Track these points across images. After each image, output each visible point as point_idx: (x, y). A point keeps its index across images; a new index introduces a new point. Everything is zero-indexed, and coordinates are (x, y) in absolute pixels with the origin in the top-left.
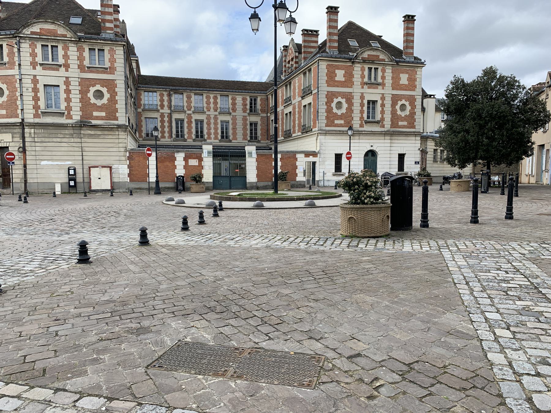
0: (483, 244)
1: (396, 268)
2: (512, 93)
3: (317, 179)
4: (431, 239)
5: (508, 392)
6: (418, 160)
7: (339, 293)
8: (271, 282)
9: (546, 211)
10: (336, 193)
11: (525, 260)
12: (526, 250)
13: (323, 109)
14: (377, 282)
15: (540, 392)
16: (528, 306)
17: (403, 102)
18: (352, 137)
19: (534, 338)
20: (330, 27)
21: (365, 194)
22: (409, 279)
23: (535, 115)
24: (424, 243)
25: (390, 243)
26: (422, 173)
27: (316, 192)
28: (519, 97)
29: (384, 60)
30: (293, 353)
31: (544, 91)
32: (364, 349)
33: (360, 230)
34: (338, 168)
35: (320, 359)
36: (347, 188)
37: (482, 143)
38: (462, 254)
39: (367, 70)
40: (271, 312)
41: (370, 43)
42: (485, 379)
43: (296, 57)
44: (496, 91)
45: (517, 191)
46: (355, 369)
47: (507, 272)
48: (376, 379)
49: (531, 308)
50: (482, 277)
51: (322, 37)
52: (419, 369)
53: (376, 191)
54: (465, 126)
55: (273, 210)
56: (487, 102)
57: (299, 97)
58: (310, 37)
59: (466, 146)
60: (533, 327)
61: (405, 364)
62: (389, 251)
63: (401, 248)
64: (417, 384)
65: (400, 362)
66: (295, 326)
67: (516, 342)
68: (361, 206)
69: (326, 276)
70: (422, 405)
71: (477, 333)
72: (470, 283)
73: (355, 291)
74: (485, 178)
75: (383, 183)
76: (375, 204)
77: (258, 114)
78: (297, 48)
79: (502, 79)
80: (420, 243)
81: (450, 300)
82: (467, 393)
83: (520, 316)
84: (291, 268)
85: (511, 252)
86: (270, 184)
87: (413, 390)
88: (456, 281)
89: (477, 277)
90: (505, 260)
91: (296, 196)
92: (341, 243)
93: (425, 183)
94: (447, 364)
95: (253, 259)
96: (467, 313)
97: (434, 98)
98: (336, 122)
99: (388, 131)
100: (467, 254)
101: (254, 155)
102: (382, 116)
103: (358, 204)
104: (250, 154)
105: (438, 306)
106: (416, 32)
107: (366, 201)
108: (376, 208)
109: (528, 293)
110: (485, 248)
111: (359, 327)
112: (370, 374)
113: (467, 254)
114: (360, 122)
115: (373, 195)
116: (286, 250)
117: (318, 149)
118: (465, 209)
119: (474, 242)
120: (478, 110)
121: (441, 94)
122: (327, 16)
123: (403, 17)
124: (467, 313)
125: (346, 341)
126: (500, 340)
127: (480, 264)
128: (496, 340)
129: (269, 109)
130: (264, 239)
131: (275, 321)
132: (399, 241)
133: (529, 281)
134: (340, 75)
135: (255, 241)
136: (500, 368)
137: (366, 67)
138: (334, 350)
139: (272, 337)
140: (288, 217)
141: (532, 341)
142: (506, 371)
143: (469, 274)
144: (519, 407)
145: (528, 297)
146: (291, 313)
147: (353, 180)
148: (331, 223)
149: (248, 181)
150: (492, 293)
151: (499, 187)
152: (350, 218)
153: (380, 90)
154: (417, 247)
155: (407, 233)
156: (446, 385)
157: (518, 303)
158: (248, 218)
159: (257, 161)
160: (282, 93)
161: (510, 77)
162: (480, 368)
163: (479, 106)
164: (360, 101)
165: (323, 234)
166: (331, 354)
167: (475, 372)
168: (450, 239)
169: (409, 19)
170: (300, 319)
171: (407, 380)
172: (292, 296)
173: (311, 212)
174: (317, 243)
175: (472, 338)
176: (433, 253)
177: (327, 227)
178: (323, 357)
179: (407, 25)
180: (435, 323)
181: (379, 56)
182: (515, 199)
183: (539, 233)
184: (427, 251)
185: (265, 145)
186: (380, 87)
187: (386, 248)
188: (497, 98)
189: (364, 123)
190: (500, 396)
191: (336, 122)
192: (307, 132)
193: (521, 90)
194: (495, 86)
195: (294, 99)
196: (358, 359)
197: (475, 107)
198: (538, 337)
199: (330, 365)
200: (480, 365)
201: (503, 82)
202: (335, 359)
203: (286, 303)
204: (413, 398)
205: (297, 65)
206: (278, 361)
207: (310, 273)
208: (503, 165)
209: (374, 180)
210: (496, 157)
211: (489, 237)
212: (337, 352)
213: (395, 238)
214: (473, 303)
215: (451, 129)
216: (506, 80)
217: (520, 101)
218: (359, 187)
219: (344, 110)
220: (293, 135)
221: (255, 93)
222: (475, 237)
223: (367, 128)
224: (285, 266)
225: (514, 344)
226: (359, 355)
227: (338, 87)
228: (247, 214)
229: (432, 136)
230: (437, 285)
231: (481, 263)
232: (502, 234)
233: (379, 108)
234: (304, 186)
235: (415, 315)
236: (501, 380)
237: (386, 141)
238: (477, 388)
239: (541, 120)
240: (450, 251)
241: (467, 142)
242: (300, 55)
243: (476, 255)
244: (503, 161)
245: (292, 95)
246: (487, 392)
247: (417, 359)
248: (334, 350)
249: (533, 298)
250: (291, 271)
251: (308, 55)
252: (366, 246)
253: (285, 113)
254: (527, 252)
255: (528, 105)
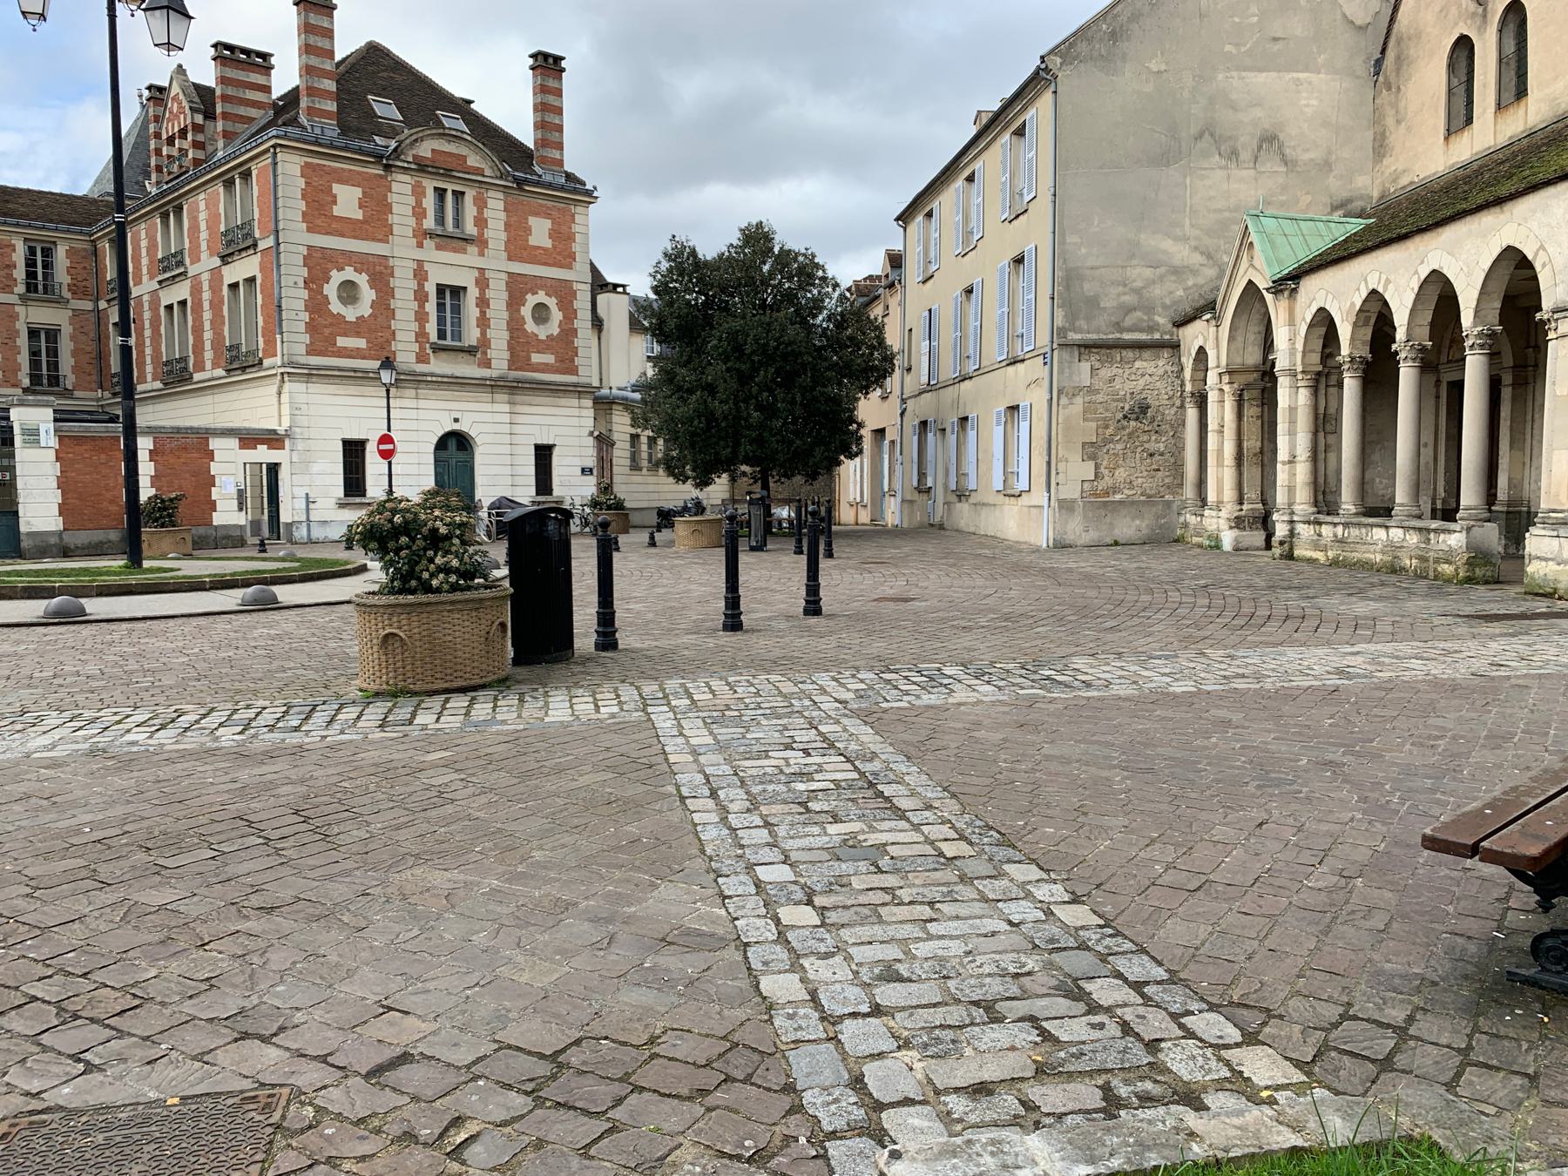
0: (752, 685)
1: (525, 776)
2: (809, 295)
3: (285, 517)
4: (623, 682)
5: (808, 1075)
6: (591, 462)
7: (347, 873)
8: (104, 871)
9: (891, 592)
10: (347, 563)
11: (846, 715)
12: (848, 690)
13: (295, 300)
14: (467, 823)
15: (880, 1055)
16: (854, 835)
17: (541, 297)
18: (393, 391)
19: (867, 917)
20: (307, 49)
21: (431, 561)
22: (560, 801)
23: (863, 355)
24: (606, 695)
25: (510, 703)
26: (603, 499)
27: (283, 560)
28: (825, 308)
29: (480, 172)
30: (176, 1101)
31: (877, 297)
32: (422, 1035)
33: (419, 670)
34: (354, 483)
35: (275, 1099)
36: (374, 545)
37: (746, 420)
38: (701, 714)
39: (430, 193)
40: (98, 976)
41: (437, 116)
42: (754, 1049)
43: (198, 128)
44: (774, 287)
45: (829, 544)
46: (392, 1106)
47: (807, 752)
48: (458, 1122)
49: (861, 837)
50: (750, 772)
51: (285, 77)
52: (584, 1063)
53: (466, 551)
54: (703, 373)
55: (125, 625)
56: (754, 315)
57: (211, 255)
58: (243, 70)
59: (709, 428)
60: (865, 886)
61: (541, 1056)
62: (506, 727)
63: (541, 714)
64: (575, 1108)
65: (530, 1053)
66: (189, 1008)
67: (827, 936)
68: (423, 598)
69: (304, 827)
70: (588, 1168)
71: (736, 927)
72: (720, 792)
73: (398, 862)
74: (758, 512)
75: (494, 529)
76: (462, 589)
77: (60, 302)
78: (197, 99)
79: (786, 257)
80: (593, 695)
81: (670, 847)
82: (710, 1100)
83: (837, 864)
84: (180, 814)
85: (817, 699)
86: (114, 535)
87: (574, 1130)
88: (685, 791)
89: (736, 774)
90: (802, 720)
91: (209, 576)
92: (359, 717)
93: (605, 525)
94: (658, 1032)
95: (33, 800)
96: (712, 876)
97: (625, 292)
98: (342, 342)
99: (501, 378)
100: (715, 714)
101: (49, 439)
102: (483, 334)
103: (413, 592)
104: (32, 434)
105: (639, 869)
106: (569, 103)
107: (435, 583)
108: (467, 601)
109: (853, 800)
110: (758, 694)
111: (406, 970)
112: (437, 1111)
113: (715, 714)
114: (416, 347)
115: (455, 563)
116: (166, 756)
117: (286, 424)
118: (711, 594)
119: (731, 679)
120: (733, 335)
121: (641, 286)
122: (299, 14)
123: (531, 56)
124: (712, 876)
125: (365, 1022)
126: (790, 936)
127: (744, 737)
128: (782, 939)
129: (104, 288)
130: (80, 728)
131: (111, 1001)
132: (535, 694)
133: (856, 769)
134: (347, 202)
135: (46, 736)
136: (791, 1011)
137: (429, 185)
138: (323, 1059)
139: (97, 1061)
140: (180, 644)
141: (862, 925)
142: (806, 1016)
143: (717, 766)
144: (833, 1107)
145: (854, 811)
146: (175, 966)
147: (391, 521)
148: (330, 657)
149: (23, 528)
150: (774, 811)
151: (790, 535)
152: (387, 636)
153: (471, 257)
154: (584, 706)
155: (560, 669)
156: (655, 1091)
157: (833, 829)
158: (22, 657)
159: (58, 459)
160: (145, 239)
161: (804, 255)
162: (742, 1024)
163: (736, 324)
164: (413, 285)
165: (301, 694)
166: (310, 1075)
167: (730, 1038)
168: (670, 678)
169: (547, 65)
170: (207, 979)
171: (548, 1104)
172: (182, 909)
173: (263, 626)
174: (280, 725)
175: (722, 943)
176: (627, 719)
177: (317, 671)
178: (285, 1091)
179: (543, 80)
180: (628, 920)
181: (464, 158)
182: (824, 564)
183: (878, 646)
184: (613, 716)
185: (91, 405)
186: (472, 249)
187: (499, 717)
188: (775, 307)
189: (429, 351)
190: (790, 1089)
191: (342, 342)
192: (243, 369)
193: (830, 289)
194: (771, 274)
195: (196, 259)
196: (402, 1074)
197: (727, 326)
198: (876, 911)
199: (309, 1112)
200: (740, 1014)
201: (787, 265)
202: (325, 1087)
203: (157, 937)
204: (563, 1154)
205: (201, 155)
206: (118, 1139)
207: (250, 823)
208: (798, 479)
209: (458, 519)
210: (781, 457)
211: (768, 664)
212: (333, 1066)
213: (525, 688)
214: (727, 849)
215: (671, 381)
216: (795, 260)
217: (829, 318)
218: (413, 539)
219: (364, 308)
220: (197, 377)
221: (43, 228)
222: (733, 668)
223: (440, 366)
224: (161, 810)
225: (822, 940)
226: (405, 1058)
227: (343, 236)
228: (18, 642)
229: (623, 399)
230: (633, 807)
231: (748, 736)
232: (795, 654)
233: (471, 310)
234: (240, 542)
235: (576, 904)
236: (792, 1046)
237: (497, 407)
238: (735, 1080)
239: (875, 368)
240: (673, 709)
241: (710, 417)
242: (209, 124)
243: (736, 713)
244: (797, 468)
245: (187, 245)
246: (760, 1087)
247: (578, 1035)
248: (323, 1059)
249: (866, 812)
250: (183, 825)
251: (239, 127)
252: (438, 720)
253: (164, 303)
254: (851, 695)
255: (846, 329)
